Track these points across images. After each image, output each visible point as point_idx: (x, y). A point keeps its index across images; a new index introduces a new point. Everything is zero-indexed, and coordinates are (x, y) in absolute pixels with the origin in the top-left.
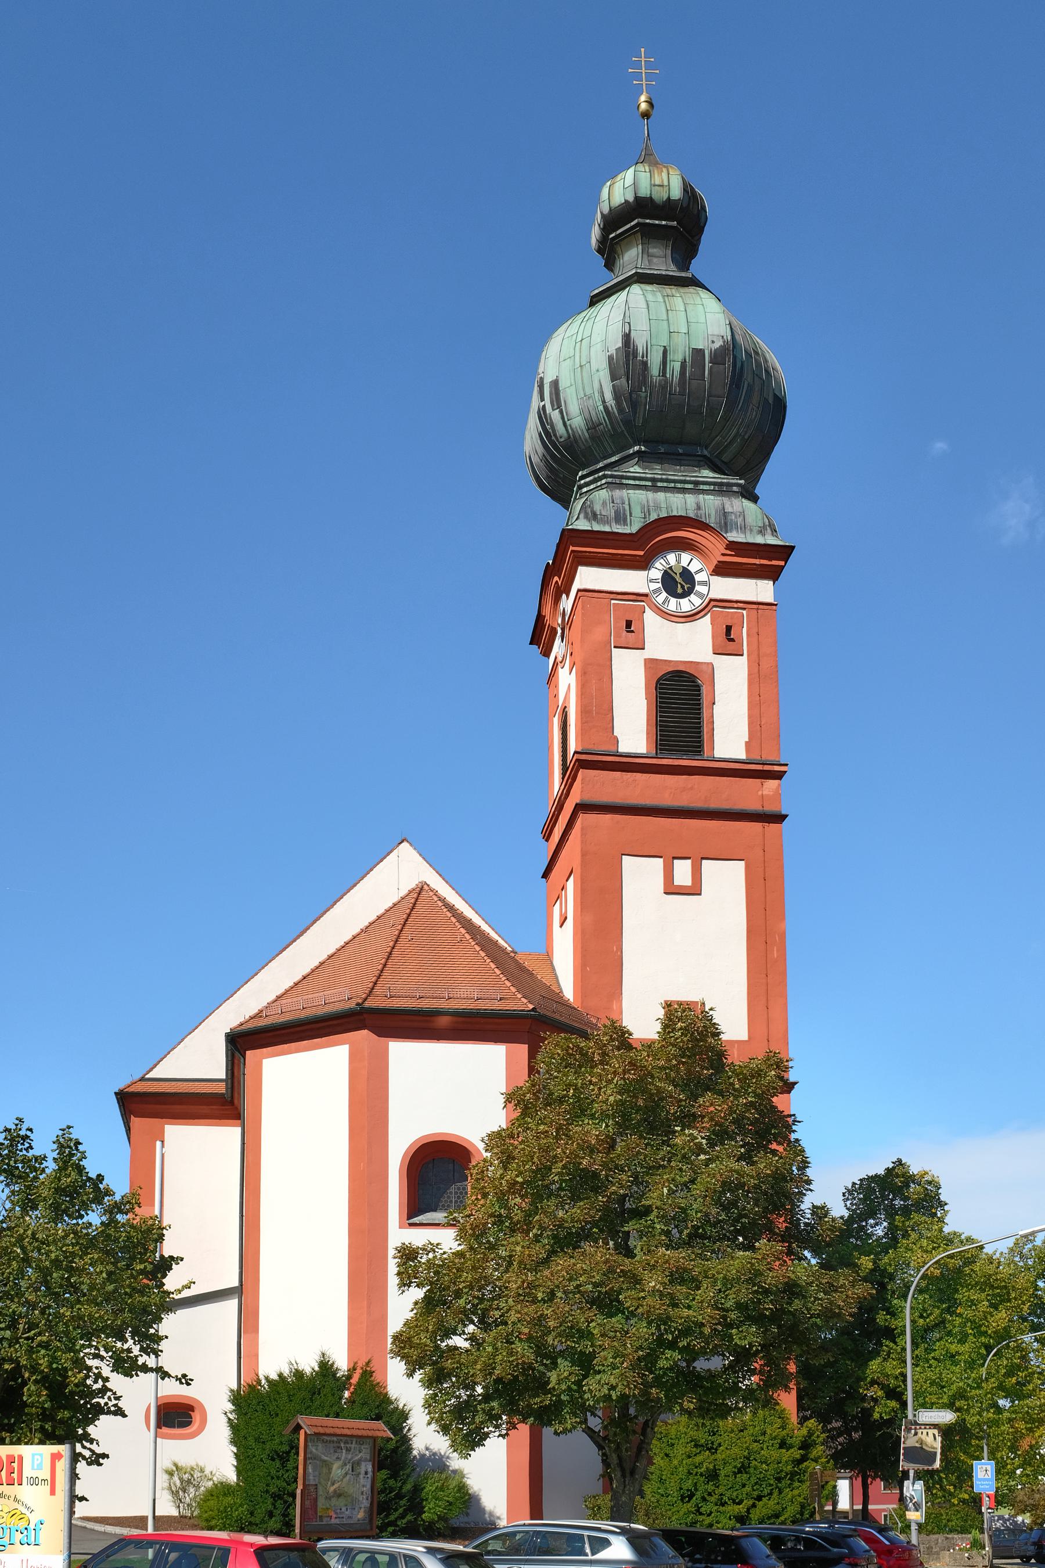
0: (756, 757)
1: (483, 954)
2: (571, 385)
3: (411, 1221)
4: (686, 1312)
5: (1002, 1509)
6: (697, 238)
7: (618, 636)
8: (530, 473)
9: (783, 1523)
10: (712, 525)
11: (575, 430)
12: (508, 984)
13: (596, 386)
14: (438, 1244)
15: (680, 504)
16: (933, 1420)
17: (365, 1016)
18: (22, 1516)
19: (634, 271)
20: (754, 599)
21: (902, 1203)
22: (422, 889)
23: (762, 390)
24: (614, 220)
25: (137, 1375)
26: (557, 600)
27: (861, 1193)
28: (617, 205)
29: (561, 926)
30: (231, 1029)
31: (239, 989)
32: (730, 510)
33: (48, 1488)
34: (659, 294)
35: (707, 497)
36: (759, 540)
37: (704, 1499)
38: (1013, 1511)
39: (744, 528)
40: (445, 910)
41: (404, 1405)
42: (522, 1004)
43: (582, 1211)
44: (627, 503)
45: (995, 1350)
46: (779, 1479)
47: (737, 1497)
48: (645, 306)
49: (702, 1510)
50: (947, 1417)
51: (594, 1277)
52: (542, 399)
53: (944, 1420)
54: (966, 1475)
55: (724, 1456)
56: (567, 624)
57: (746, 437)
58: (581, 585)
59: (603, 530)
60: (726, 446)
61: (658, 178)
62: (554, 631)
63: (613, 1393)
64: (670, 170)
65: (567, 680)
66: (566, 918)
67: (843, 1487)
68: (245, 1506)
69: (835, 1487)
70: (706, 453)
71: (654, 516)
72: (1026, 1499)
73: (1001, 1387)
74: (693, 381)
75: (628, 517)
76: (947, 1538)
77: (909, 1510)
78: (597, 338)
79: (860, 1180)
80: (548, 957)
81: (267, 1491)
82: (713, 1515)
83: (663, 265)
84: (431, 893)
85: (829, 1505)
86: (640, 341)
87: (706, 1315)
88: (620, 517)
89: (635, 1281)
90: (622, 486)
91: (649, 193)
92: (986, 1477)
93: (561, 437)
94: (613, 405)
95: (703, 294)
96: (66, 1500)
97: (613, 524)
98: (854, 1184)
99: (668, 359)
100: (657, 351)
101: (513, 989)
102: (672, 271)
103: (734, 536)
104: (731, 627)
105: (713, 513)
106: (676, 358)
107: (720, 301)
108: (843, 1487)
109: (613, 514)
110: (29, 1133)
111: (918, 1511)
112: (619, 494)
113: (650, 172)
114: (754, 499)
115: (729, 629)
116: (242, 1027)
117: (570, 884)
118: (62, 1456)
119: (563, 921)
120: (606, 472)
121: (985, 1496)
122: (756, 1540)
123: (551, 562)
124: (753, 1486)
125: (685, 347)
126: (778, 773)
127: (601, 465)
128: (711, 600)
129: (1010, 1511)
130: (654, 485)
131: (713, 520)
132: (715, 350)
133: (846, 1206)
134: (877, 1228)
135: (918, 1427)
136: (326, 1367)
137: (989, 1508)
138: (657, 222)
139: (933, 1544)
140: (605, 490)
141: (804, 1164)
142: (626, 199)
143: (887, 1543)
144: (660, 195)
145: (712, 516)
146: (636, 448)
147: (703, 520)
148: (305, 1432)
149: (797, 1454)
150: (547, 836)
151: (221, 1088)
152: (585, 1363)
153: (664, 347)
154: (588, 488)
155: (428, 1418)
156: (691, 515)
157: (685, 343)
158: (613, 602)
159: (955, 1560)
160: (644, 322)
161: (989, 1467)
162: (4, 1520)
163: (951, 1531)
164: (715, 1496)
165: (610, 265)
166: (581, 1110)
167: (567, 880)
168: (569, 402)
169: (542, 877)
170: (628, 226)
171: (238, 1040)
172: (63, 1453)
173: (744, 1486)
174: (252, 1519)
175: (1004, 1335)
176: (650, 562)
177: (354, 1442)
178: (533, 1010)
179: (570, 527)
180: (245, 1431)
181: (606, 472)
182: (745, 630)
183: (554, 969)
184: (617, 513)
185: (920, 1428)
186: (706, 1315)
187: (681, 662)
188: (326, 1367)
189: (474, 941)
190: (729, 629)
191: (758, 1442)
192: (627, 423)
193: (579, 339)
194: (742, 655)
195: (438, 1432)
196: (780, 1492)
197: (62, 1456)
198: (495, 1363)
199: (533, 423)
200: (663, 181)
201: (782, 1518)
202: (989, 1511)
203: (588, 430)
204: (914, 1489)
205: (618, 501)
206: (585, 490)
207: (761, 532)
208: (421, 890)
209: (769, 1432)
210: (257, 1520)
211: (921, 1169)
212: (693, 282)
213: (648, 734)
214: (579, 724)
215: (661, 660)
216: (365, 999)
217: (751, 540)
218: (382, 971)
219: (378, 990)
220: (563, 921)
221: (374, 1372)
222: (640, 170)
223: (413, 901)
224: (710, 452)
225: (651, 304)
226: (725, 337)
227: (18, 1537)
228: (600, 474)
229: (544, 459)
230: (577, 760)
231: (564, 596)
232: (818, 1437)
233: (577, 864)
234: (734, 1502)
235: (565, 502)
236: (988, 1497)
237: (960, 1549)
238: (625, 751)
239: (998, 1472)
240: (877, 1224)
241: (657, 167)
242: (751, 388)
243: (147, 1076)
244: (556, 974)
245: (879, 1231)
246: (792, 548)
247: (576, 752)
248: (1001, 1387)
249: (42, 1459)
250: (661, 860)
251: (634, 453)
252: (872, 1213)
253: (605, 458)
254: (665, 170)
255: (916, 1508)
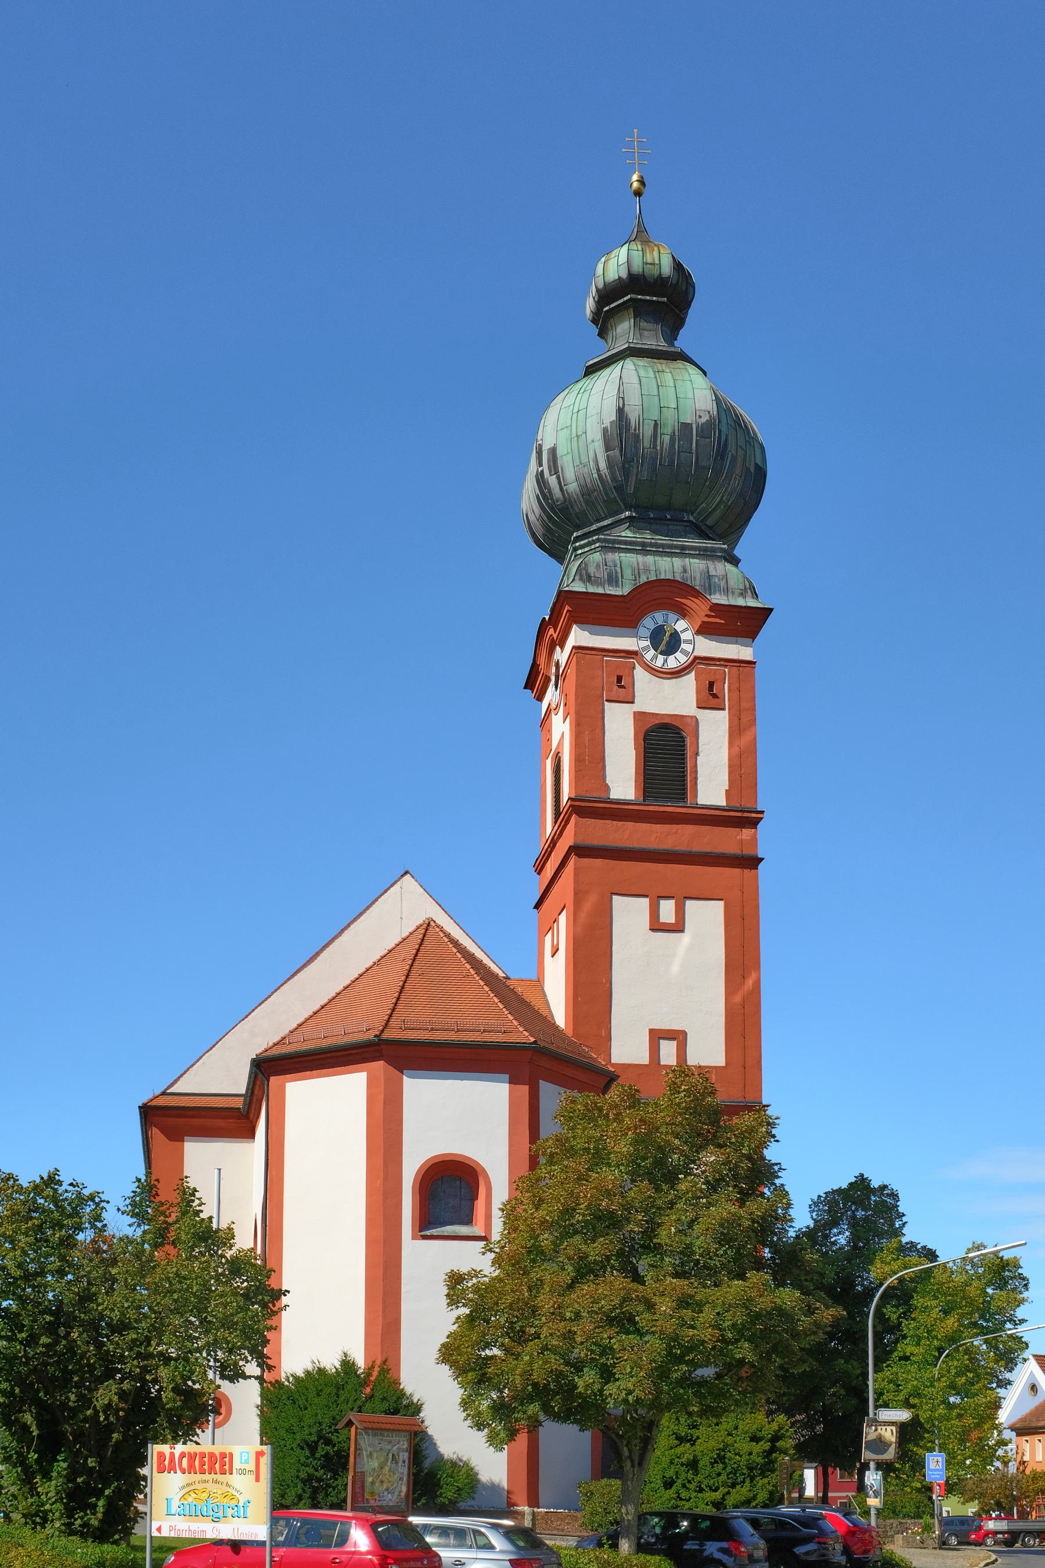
0: (735, 804)
1: (486, 988)
2: (568, 453)
3: (422, 1233)
4: (691, 1332)
5: (952, 1497)
6: (685, 311)
7: (610, 690)
8: (526, 530)
9: (754, 1507)
10: (697, 588)
11: (571, 494)
12: (511, 1017)
13: (591, 455)
14: (480, 1271)
15: (667, 567)
16: (891, 1418)
17: (383, 1047)
18: (233, 1497)
19: (627, 346)
20: (735, 657)
21: (863, 1213)
22: (429, 924)
23: (744, 460)
24: (608, 294)
25: (238, 1382)
26: (551, 652)
27: (825, 1205)
28: (611, 281)
29: (553, 956)
30: (256, 1055)
31: (253, 1010)
32: (714, 573)
33: (254, 1477)
34: (650, 369)
35: (692, 561)
36: (740, 602)
37: (684, 1486)
38: (962, 1499)
39: (727, 591)
40: (451, 946)
41: (419, 1400)
42: (525, 1037)
43: (602, 1245)
44: (619, 566)
45: (947, 1351)
46: (750, 1469)
47: (714, 1485)
48: (638, 382)
49: (683, 1496)
50: (903, 1415)
51: (613, 1300)
52: (541, 465)
53: (901, 1418)
54: (919, 1466)
55: (702, 1448)
56: (562, 676)
57: (729, 503)
58: (576, 642)
59: (597, 592)
60: (710, 513)
61: (652, 256)
62: (547, 680)
63: (630, 1398)
64: (661, 249)
65: (561, 728)
66: (558, 949)
67: (809, 1475)
68: (277, 1490)
69: (802, 1475)
70: (691, 518)
71: (643, 579)
72: (974, 1487)
73: (952, 1386)
74: (681, 453)
75: (620, 579)
76: (901, 1523)
77: (870, 1497)
78: (593, 410)
79: (826, 1193)
80: (539, 983)
81: (298, 1477)
82: (692, 1500)
83: (655, 341)
84: (438, 930)
85: (796, 1492)
86: (633, 415)
87: (707, 1334)
88: (613, 579)
89: (650, 1306)
90: (614, 550)
91: (641, 270)
92: (938, 1467)
93: (558, 501)
94: (607, 473)
95: (692, 370)
96: (269, 1486)
97: (606, 586)
98: (819, 1197)
99: (659, 432)
100: (648, 425)
101: (515, 1023)
102: (662, 345)
103: (718, 599)
104: (713, 682)
105: (698, 576)
106: (666, 432)
107: (705, 373)
108: (809, 1475)
109: (606, 576)
110: (156, 1183)
111: (877, 1498)
112: (612, 557)
113: (642, 250)
114: (735, 561)
115: (711, 685)
116: (268, 1053)
117: (563, 919)
118: (264, 1454)
119: (555, 951)
120: (600, 537)
121: (935, 1484)
122: (742, 1521)
123: (547, 618)
124: (728, 1475)
125: (674, 422)
126: (755, 820)
127: (594, 527)
128: (696, 658)
129: (959, 1499)
130: (644, 549)
131: (698, 582)
132: (702, 424)
133: (812, 1217)
134: (841, 1236)
135: (878, 1424)
136: (347, 1365)
137: (940, 1496)
138: (648, 298)
139: (888, 1528)
140: (598, 553)
141: (789, 1205)
142: (621, 275)
143: (851, 1525)
144: (652, 272)
145: (697, 578)
146: (627, 513)
147: (689, 583)
148: (356, 1427)
149: (767, 1446)
150: (539, 869)
151: (239, 1103)
152: (607, 1375)
153: (655, 421)
154: (583, 551)
155: (465, 1414)
156: (678, 578)
157: (675, 417)
158: (605, 658)
159: (908, 1542)
160: (637, 397)
161: (940, 1459)
162: (218, 1499)
163: (904, 1517)
164: (694, 1484)
165: (602, 334)
166: (599, 1157)
167: (559, 915)
168: (566, 469)
169: (534, 908)
170: (621, 301)
171: (263, 1065)
172: (265, 1451)
173: (719, 1474)
174: (283, 1502)
175: (953, 1339)
176: (640, 621)
177: (394, 1435)
178: (535, 1042)
179: (566, 589)
180: (277, 1424)
181: (600, 537)
182: (726, 685)
183: (545, 995)
184: (610, 575)
185: (880, 1425)
186: (707, 1334)
187: (667, 715)
188: (347, 1365)
189: (478, 976)
190: (711, 685)
191: (731, 1435)
192: (619, 489)
193: (576, 410)
194: (723, 709)
195: (472, 1427)
196: (752, 1481)
197: (264, 1454)
198: (532, 1370)
199: (530, 486)
200: (654, 260)
201: (754, 1504)
202: (940, 1498)
203: (583, 495)
204: (873, 1478)
205: (611, 564)
206: (580, 552)
207: (743, 594)
208: (428, 926)
209: (740, 1427)
210: (288, 1502)
211: (881, 1184)
212: (681, 357)
213: (636, 782)
214: (574, 773)
215: (649, 713)
216: (382, 1031)
217: (733, 602)
218: (396, 1004)
219: (393, 1023)
220: (555, 951)
221: (390, 1369)
222: (633, 248)
223: (421, 936)
224: (695, 518)
225: (643, 380)
226: (711, 413)
227: (230, 1512)
228: (594, 538)
229: (540, 519)
230: (571, 806)
231: (558, 648)
232: (787, 1430)
233: (570, 901)
234: (711, 1489)
235: (560, 558)
236: (939, 1486)
237: (913, 1533)
238: (615, 798)
239: (948, 1463)
240: (839, 1233)
241: (649, 246)
242: (734, 459)
243: (168, 1091)
244: (547, 1000)
245: (842, 1240)
246: (771, 610)
247: (569, 799)
248: (952, 1386)
249: (248, 1457)
250: (647, 900)
251: (626, 518)
252: (835, 1223)
253: (598, 521)
254: (656, 249)
255: (875, 1495)
